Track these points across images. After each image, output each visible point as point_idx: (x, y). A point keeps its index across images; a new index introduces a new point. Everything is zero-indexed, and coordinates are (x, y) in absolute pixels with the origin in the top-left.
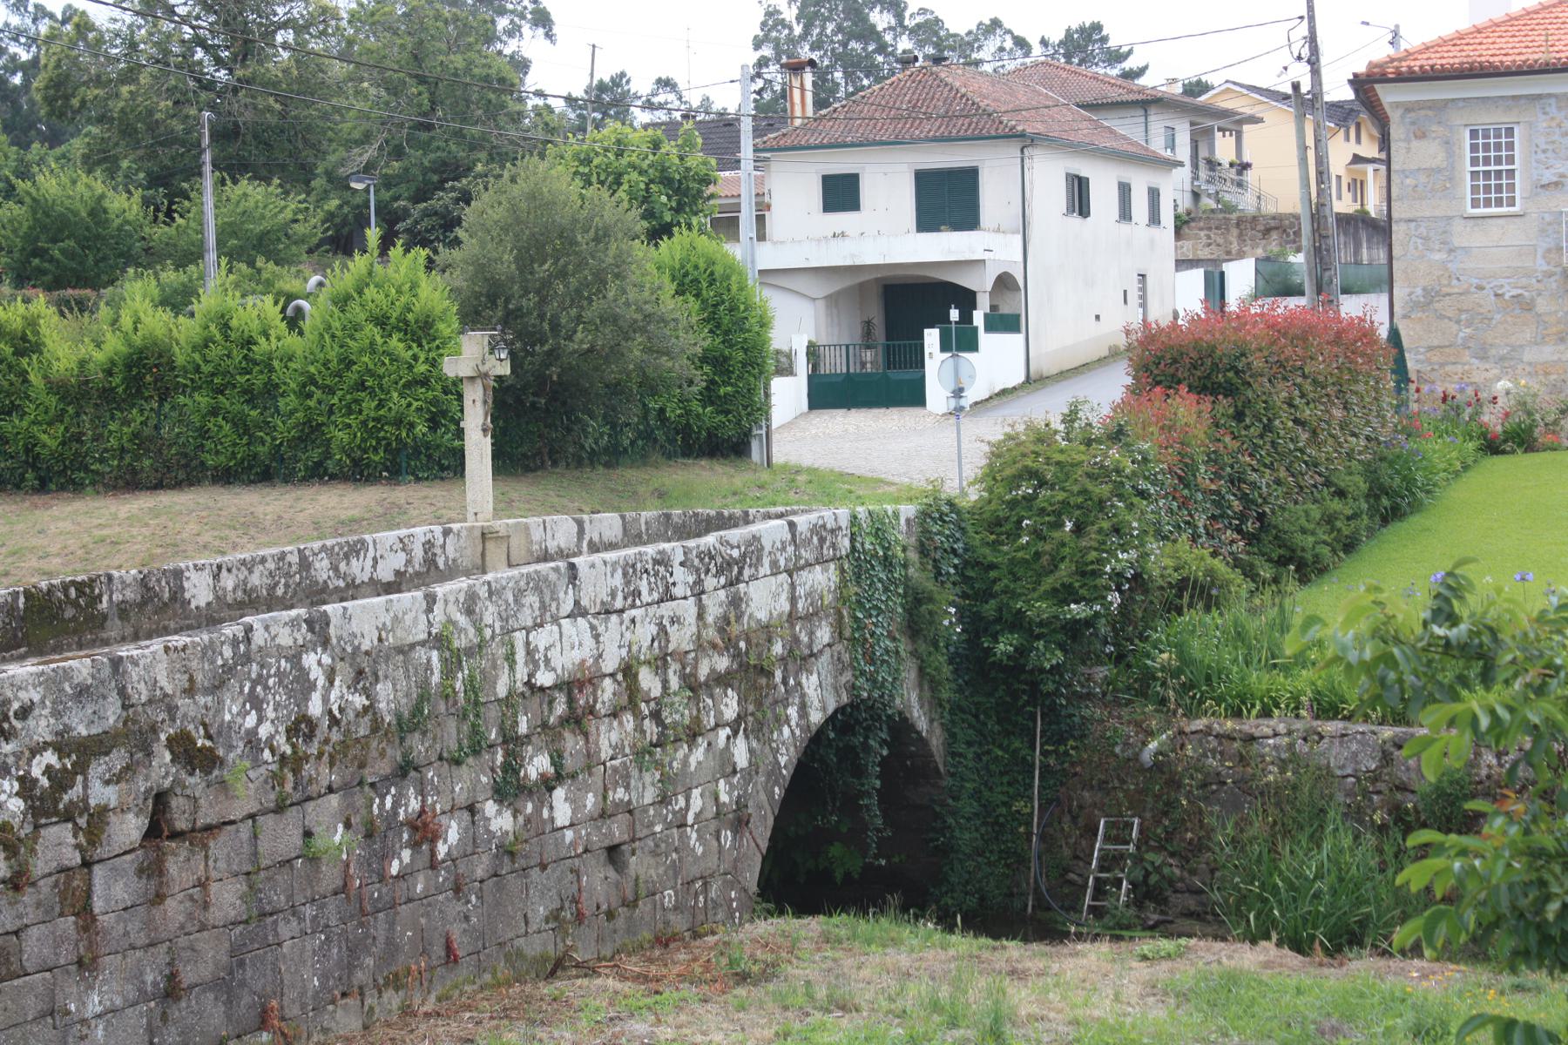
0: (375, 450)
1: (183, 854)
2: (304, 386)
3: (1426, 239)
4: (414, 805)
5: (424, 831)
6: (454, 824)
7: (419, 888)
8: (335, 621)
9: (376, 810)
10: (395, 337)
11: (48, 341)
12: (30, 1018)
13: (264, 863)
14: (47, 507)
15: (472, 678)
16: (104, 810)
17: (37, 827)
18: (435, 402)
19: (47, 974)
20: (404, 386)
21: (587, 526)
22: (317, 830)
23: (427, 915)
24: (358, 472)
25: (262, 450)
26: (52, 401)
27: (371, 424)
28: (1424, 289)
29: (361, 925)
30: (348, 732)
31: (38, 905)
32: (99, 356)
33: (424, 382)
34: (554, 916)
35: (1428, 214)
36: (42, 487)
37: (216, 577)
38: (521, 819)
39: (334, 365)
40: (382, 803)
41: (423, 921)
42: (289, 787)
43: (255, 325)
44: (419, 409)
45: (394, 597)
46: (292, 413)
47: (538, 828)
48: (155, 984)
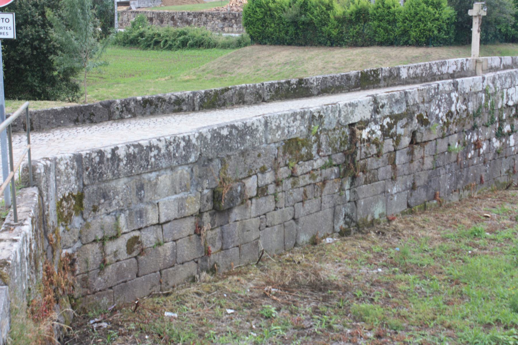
0: (423, 38)
1: (419, 149)
2: (404, 20)
4: (476, 138)
5: (477, 145)
6: (485, 144)
7: (475, 162)
8: (460, 84)
9: (466, 138)
10: (430, 7)
11: (335, 7)
12: (379, 193)
13: (438, 152)
14: (334, 51)
15: (492, 102)
16: (400, 135)
17: (384, 139)
18: (440, 25)
19: (384, 181)
20: (432, 20)
21: (503, 60)
22: (451, 144)
23: (476, 169)
24: (418, 44)
25: (391, 37)
26: (336, 23)
27: (422, 31)
29: (460, 171)
30: (461, 116)
31: (383, 161)
32: (349, 11)
33: (437, 19)
34: (508, 172)
36: (332, 45)
37: (408, 70)
38: (502, 143)
39: (413, 14)
40: (468, 137)
41: (475, 171)
42: (445, 131)
43: (391, 3)
44: (435, 27)
45: (474, 77)
46: (400, 27)
47: (505, 146)
48: (410, 185)
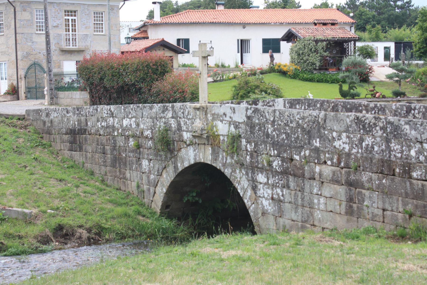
3: (26, 39)
28: (26, 53)
35: (27, 32)
